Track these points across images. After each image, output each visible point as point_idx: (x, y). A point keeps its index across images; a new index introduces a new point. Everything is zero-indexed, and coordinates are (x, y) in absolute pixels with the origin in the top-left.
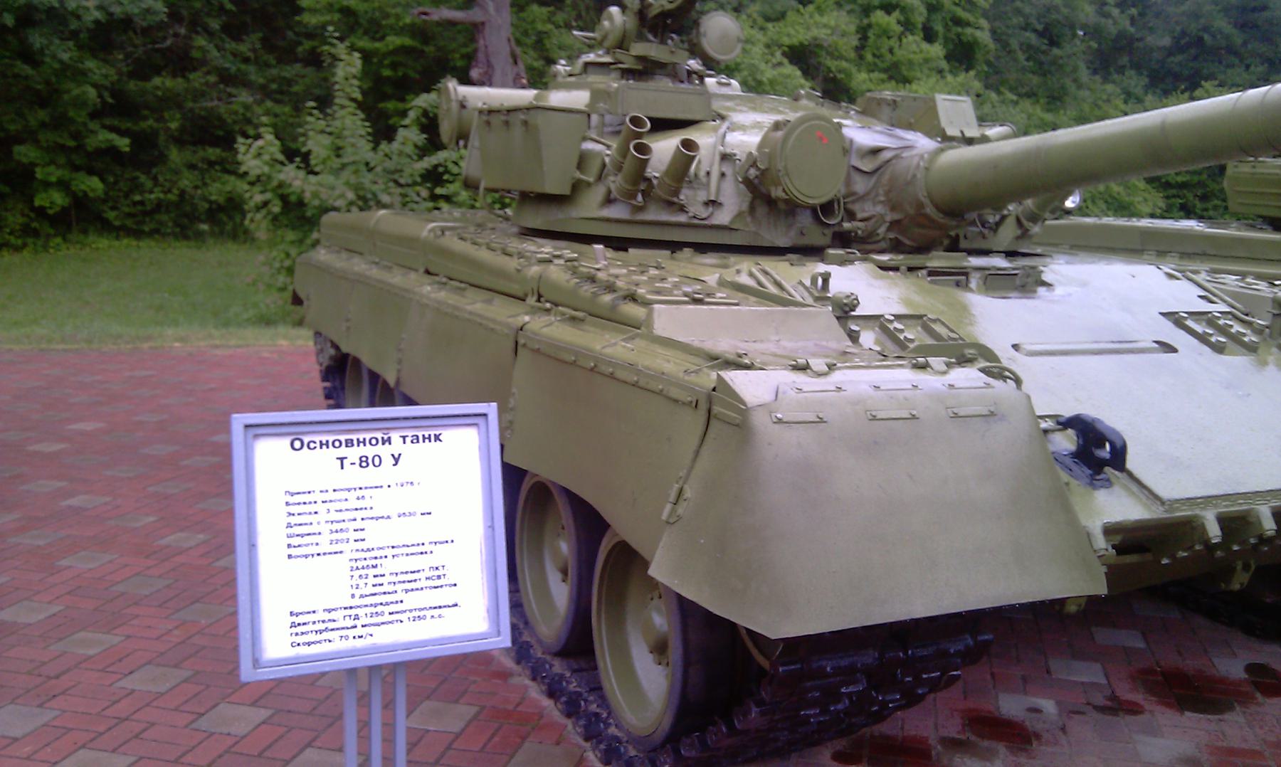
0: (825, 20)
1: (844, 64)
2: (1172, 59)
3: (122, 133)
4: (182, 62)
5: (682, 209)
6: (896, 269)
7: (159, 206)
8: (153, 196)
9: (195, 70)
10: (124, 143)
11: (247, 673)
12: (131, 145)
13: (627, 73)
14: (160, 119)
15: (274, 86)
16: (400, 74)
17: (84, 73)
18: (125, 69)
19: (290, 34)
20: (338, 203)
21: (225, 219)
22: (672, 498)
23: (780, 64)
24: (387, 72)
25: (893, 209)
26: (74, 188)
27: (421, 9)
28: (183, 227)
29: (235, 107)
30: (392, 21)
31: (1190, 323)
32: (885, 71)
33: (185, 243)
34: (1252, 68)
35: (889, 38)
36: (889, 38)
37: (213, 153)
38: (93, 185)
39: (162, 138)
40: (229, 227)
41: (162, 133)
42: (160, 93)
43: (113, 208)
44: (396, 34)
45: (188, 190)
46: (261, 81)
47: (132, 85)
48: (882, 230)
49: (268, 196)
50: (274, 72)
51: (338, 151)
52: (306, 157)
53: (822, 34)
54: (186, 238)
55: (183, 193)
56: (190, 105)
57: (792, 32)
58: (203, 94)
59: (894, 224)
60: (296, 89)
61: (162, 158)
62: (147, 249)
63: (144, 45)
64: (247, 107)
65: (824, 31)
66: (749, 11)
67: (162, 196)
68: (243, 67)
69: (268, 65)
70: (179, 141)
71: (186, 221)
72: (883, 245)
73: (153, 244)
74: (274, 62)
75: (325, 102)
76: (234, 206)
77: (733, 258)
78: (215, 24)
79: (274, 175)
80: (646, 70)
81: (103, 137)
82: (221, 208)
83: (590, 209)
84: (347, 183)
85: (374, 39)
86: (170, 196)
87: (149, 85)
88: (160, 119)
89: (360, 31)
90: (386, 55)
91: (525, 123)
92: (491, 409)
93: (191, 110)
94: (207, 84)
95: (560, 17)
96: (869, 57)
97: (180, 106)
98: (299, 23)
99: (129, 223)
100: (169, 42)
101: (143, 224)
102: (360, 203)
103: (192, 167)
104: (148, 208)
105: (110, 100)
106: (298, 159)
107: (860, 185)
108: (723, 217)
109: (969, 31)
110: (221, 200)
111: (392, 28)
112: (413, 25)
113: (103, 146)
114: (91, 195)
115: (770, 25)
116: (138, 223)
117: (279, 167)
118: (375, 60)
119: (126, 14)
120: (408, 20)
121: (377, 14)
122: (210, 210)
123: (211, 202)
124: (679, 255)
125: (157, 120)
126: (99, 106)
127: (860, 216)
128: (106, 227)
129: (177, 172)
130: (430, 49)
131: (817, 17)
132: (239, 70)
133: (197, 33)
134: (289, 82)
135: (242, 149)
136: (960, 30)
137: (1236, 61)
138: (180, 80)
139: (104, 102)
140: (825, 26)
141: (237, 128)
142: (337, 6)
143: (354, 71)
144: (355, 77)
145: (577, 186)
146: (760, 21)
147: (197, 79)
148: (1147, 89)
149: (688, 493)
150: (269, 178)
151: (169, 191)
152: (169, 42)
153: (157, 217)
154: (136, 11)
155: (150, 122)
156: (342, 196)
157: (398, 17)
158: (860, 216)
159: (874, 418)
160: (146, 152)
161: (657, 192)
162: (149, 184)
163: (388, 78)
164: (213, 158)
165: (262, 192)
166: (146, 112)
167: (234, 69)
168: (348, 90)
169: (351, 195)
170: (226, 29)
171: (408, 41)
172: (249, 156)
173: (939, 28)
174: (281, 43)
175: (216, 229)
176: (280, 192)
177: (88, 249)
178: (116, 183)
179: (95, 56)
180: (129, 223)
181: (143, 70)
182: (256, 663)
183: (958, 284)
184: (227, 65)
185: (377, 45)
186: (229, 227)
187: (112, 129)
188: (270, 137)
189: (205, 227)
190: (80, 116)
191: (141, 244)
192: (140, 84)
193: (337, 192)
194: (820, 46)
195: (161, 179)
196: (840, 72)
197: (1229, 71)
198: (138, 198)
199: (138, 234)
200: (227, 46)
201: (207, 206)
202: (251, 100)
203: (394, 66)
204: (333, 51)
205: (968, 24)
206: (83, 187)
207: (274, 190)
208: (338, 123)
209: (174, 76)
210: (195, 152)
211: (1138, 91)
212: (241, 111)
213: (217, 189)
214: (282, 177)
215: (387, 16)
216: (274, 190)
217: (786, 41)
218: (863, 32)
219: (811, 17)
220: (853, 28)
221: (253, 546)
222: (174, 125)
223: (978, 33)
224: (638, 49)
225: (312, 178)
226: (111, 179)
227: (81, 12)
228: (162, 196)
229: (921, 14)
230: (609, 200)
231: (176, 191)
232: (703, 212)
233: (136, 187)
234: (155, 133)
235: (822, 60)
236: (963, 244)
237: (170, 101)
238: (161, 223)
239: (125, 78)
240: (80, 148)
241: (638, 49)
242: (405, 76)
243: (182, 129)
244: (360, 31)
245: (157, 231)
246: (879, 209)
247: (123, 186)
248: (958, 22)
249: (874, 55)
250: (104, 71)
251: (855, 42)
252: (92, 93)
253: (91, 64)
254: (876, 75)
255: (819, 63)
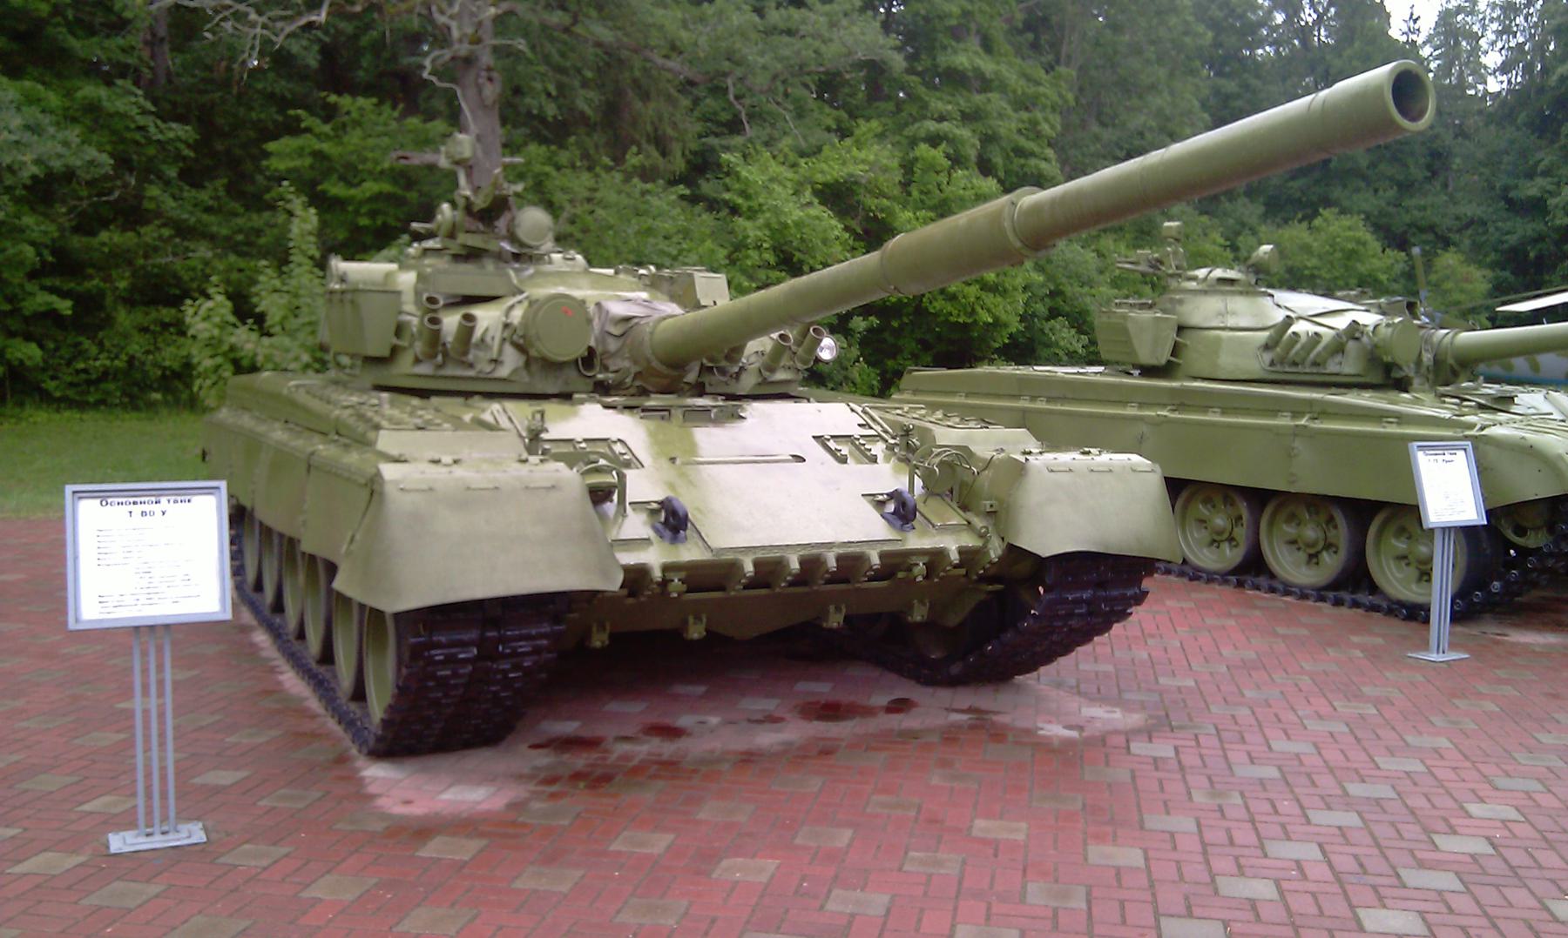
0: (862, 155)
1: (885, 202)
2: (1291, 184)
3: (63, 294)
4: (132, 215)
5: (471, 366)
6: (614, 408)
7: (105, 375)
8: (98, 363)
9: (148, 222)
10: (65, 306)
11: (72, 625)
12: (74, 308)
13: (457, 258)
14: (107, 279)
15: (240, 237)
16: (379, 222)
17: (22, 230)
18: (67, 225)
19: (259, 178)
20: (292, 366)
21: (181, 386)
22: (348, 539)
23: (810, 204)
24: (364, 221)
25: (635, 362)
26: (8, 356)
27: (400, 153)
28: (132, 397)
29: (191, 263)
30: (369, 165)
31: (832, 444)
32: (931, 209)
33: (135, 415)
34: (1381, 192)
35: (937, 173)
36: (937, 173)
37: (167, 314)
38: (30, 353)
39: (109, 300)
40: (184, 396)
41: (109, 293)
42: (106, 250)
43: (53, 378)
44: (375, 180)
45: (138, 355)
46: (225, 231)
47: (76, 242)
48: (628, 380)
49: (219, 360)
50: (240, 221)
51: (295, 311)
52: (260, 319)
53: (857, 170)
54: (136, 408)
55: (132, 358)
56: (141, 262)
57: (824, 167)
58: (156, 249)
59: (638, 375)
60: (262, 241)
61: (109, 322)
62: (91, 422)
63: (90, 197)
64: (207, 263)
65: (861, 167)
66: (780, 145)
67: (108, 363)
68: (205, 217)
69: (236, 215)
70: (129, 302)
71: (136, 389)
72: (632, 391)
73: (98, 416)
74: (242, 210)
75: (282, 260)
76: (184, 373)
77: (404, 398)
78: (172, 172)
79: (225, 338)
80: (472, 255)
81: (41, 300)
82: (177, 375)
83: (406, 369)
84: (303, 346)
85: (350, 185)
86: (117, 362)
87: (95, 241)
88: (107, 279)
89: (335, 177)
90: (361, 203)
91: (352, 302)
92: (223, 484)
93: (143, 267)
94: (160, 238)
95: (564, 157)
96: (915, 193)
97: (130, 263)
98: (268, 168)
99: (71, 393)
100: (116, 194)
101: (88, 394)
102: (317, 366)
103: (144, 330)
104: (94, 376)
105: (50, 259)
106: (250, 321)
107: (613, 345)
108: (504, 372)
109: (1033, 162)
110: (176, 366)
111: (370, 173)
112: (392, 169)
113: (42, 309)
114: (28, 363)
115: (802, 161)
116: (82, 393)
117: (230, 329)
118: (350, 208)
119: (67, 166)
120: (386, 165)
121: (354, 157)
122: (164, 376)
123: (164, 369)
124: (470, 401)
125: (104, 280)
126: (38, 266)
127: (612, 368)
128: (46, 398)
129: (126, 336)
130: (412, 196)
131: (855, 151)
132: (199, 221)
133: (151, 182)
134: (258, 232)
135: (190, 311)
136: (1022, 161)
137: (1362, 184)
138: (130, 234)
139: (44, 262)
140: (863, 161)
141: (194, 285)
142: (308, 150)
143: (309, 227)
144: (310, 233)
145: (395, 351)
146: (792, 157)
147: (149, 233)
148: (1264, 217)
149: (358, 537)
150: (220, 341)
151: (117, 357)
152: (116, 194)
153: (103, 386)
154: (79, 163)
155: (96, 282)
156: (297, 359)
157: (376, 162)
158: (612, 368)
159: (468, 488)
160: (90, 315)
161: (452, 354)
162: (94, 350)
163: (365, 228)
164: (167, 320)
165: (212, 357)
166: (90, 271)
167: (193, 220)
168: (304, 247)
169: (306, 358)
170: (184, 175)
171: (386, 187)
172: (198, 318)
173: (998, 160)
174: (250, 188)
175: (170, 398)
176: (232, 355)
177: (24, 424)
178: (57, 349)
179: (33, 210)
180: (71, 393)
181: (87, 224)
182: (77, 620)
183: (663, 418)
184: (185, 216)
185: (353, 192)
186: (184, 396)
187: (52, 290)
188: (220, 298)
189: (157, 396)
190: (16, 278)
191: (85, 416)
192: (85, 239)
193: (291, 356)
194: (856, 183)
195: (107, 344)
196: (882, 211)
197: (1355, 197)
198: (81, 365)
199: (82, 406)
200: (186, 194)
201: (159, 373)
202: (210, 254)
203: (373, 214)
204: (288, 206)
205: (1033, 154)
206: (19, 355)
207: (225, 354)
208: (294, 282)
209: (124, 230)
210: (147, 314)
211: (1253, 221)
212: (200, 267)
213: (169, 356)
214: (233, 340)
215: (365, 160)
216: (225, 354)
217: (819, 178)
218: (908, 167)
219: (849, 152)
220: (895, 163)
221: (76, 558)
222: (122, 284)
223: (1043, 165)
224: (463, 238)
225: (266, 341)
226: (51, 345)
227: (16, 167)
228: (108, 363)
229: (973, 146)
230: (417, 361)
231: (124, 357)
232: (488, 368)
233: (79, 353)
234: (101, 294)
235: (861, 198)
236: (708, 389)
237: (120, 257)
238: (107, 393)
239: (67, 234)
240: (15, 312)
241: (463, 238)
242: (385, 224)
243: (133, 288)
244: (335, 177)
245: (102, 402)
246: (626, 364)
247: (65, 352)
248: (1020, 152)
249: (922, 192)
250: (43, 228)
251: (898, 176)
252: (29, 251)
253: (28, 220)
254: (922, 214)
255: (858, 202)
